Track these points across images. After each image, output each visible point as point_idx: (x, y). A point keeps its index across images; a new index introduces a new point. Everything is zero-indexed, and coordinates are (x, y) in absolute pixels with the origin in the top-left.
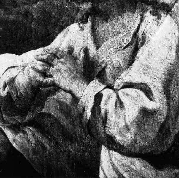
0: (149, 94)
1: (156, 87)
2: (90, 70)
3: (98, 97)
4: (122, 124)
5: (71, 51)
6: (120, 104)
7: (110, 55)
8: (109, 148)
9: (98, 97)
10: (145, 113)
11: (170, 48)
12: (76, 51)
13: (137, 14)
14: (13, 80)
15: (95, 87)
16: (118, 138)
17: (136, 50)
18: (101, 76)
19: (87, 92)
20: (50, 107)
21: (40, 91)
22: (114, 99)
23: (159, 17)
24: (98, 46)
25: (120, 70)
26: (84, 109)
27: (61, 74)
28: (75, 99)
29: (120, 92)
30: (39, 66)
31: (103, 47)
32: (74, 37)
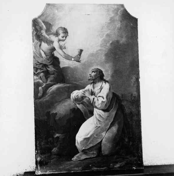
0: (103, 98)
1: (105, 97)
2: (92, 93)
3: (94, 99)
4: (98, 104)
5: (89, 90)
6: (98, 100)
7: (96, 90)
8: (96, 108)
9: (94, 99)
10: (102, 102)
11: (108, 89)
12: (90, 90)
13: (102, 83)
14: (78, 95)
15: (93, 97)
16: (97, 106)
17: (101, 90)
18: (94, 95)
19: (92, 98)
20: (85, 100)
21: (83, 97)
22: (97, 99)
23: (106, 83)
24: (94, 89)
25: (98, 93)
26: (91, 101)
27: (87, 94)
28: (89, 99)
29: (98, 98)
30: (83, 92)
31: (95, 89)
32: (89, 87)
